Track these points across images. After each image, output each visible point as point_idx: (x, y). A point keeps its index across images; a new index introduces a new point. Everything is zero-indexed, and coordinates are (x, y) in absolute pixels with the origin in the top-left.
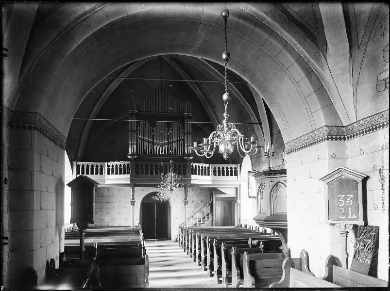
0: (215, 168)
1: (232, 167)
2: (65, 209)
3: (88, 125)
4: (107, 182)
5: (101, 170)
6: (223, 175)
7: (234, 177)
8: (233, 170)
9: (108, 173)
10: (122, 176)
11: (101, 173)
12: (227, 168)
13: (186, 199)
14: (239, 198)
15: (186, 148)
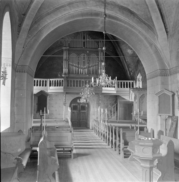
8: (131, 84)
9: (50, 86)
11: (46, 86)
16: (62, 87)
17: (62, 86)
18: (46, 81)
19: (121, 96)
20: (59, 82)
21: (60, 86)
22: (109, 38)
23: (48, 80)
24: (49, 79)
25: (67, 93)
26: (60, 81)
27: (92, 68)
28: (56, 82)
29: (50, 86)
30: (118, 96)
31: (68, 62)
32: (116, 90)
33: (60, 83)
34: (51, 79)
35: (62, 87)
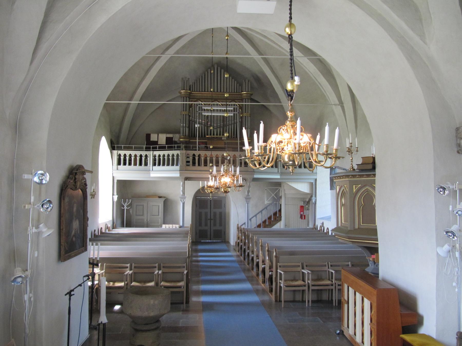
9: (154, 164)
11: (146, 164)
13: (248, 195)
14: (314, 196)
16: (178, 168)
17: (177, 165)
18: (146, 156)
21: (173, 165)
23: (150, 154)
25: (187, 179)
26: (173, 155)
28: (171, 158)
29: (154, 164)
34: (120, 152)
35: (178, 168)
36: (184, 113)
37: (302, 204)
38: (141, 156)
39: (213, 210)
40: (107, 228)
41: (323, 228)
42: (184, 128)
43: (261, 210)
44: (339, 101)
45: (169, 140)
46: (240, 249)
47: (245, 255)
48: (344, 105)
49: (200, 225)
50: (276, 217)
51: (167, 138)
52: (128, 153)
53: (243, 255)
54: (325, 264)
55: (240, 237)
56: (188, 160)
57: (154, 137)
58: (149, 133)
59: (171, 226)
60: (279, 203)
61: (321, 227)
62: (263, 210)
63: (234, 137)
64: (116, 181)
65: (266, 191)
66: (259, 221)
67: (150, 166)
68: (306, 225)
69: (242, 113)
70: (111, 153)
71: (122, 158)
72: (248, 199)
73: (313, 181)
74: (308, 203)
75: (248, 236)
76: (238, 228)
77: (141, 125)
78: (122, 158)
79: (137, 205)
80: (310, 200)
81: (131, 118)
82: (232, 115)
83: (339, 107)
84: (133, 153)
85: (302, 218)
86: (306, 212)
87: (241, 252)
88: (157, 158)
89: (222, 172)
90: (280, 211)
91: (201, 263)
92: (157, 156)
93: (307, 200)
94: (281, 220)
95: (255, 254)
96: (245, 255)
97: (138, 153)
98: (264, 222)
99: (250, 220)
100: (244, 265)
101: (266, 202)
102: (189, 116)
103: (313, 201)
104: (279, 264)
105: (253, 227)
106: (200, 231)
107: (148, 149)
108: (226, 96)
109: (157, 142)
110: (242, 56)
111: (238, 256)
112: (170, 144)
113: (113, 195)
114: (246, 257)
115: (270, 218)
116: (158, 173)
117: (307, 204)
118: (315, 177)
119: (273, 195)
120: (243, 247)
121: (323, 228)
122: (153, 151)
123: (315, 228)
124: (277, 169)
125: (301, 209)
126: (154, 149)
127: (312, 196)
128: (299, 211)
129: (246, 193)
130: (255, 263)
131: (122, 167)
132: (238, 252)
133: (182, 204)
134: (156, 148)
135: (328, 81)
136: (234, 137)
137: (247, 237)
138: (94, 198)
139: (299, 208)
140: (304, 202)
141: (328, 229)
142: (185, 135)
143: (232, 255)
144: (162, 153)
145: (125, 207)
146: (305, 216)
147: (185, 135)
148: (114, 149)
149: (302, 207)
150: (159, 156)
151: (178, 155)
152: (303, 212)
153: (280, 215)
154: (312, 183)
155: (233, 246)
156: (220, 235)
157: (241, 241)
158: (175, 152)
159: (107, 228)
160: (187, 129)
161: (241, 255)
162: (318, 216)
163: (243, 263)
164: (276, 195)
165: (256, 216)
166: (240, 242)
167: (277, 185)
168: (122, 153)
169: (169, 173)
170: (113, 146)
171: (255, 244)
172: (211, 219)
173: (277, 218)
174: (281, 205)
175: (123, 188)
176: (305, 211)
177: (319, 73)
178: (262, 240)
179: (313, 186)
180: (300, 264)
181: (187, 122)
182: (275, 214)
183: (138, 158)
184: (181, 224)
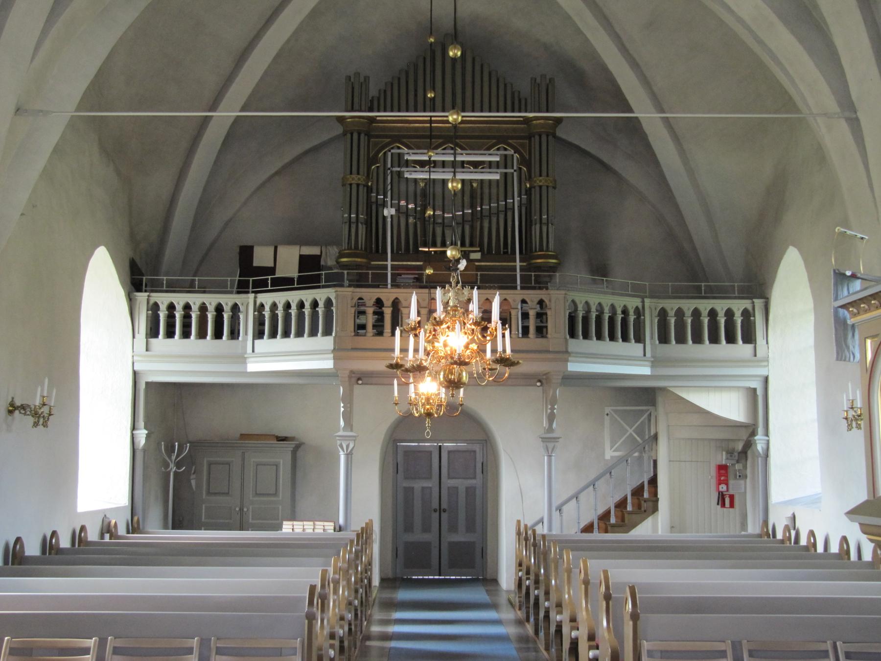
0: (663, 314)
1: (685, 309)
2: (383, 437)
3: (213, 137)
4: (253, 366)
5: (235, 319)
6: (714, 339)
7: (741, 349)
8: (738, 320)
9: (259, 334)
10: (306, 342)
11: (234, 334)
12: (713, 314)
13: (550, 429)
14: (760, 430)
15: (536, 229)
17: (327, 332)
18: (235, 308)
19: (671, 389)
20: (280, 312)
21: (313, 333)
22: (795, 105)
23: (248, 302)
24: (252, 296)
25: (360, 378)
27: (494, 220)
30: (663, 389)
31: (369, 190)
32: (648, 354)
33: (274, 317)
34: (157, 297)
36: (355, 179)
37: (722, 459)
38: (219, 309)
39: (447, 483)
40: (107, 529)
41: (793, 533)
42: (354, 226)
43: (592, 476)
44: (840, 104)
45: (308, 263)
46: (523, 599)
47: (537, 620)
48: (860, 115)
49: (409, 528)
50: (643, 500)
51: (302, 257)
52: (179, 300)
53: (532, 619)
54: (822, 647)
55: (532, 569)
56: (361, 320)
57: (262, 257)
58: (250, 244)
59: (309, 526)
60: (649, 457)
61: (787, 529)
62: (598, 478)
63: (506, 253)
64: (142, 387)
65: (607, 419)
66: (590, 515)
67: (245, 340)
68: (738, 525)
69: (530, 178)
70: (131, 300)
71: (163, 315)
72: (549, 440)
73: (757, 384)
74: (744, 453)
75: (546, 554)
76: (519, 533)
77: (227, 224)
78: (163, 315)
79: (210, 464)
80: (749, 444)
81: (196, 203)
82: (497, 177)
83: (844, 124)
84: (195, 300)
85: (723, 505)
86: (734, 486)
87: (528, 608)
88: (267, 313)
89: (439, 313)
90: (653, 481)
91: (394, 644)
92: (267, 308)
93: (740, 446)
94: (655, 509)
95: (553, 596)
96: (537, 620)
97: (211, 300)
98: (605, 516)
99: (560, 509)
100: (537, 650)
101: (610, 454)
102: (369, 190)
103: (760, 447)
104: (646, 645)
105: (573, 532)
106: (409, 546)
107: (242, 288)
108: (451, 54)
109: (272, 270)
110: (622, 422)
111: (519, 623)
112: (311, 273)
113: (134, 428)
114: (541, 624)
115: (621, 505)
116: (271, 359)
117: (738, 456)
118: (763, 372)
119: (630, 431)
120: (534, 592)
121: (793, 533)
122: (256, 292)
123: (768, 533)
124: (641, 346)
125: (719, 475)
126: (260, 287)
127: (754, 433)
128: (714, 482)
129: (545, 424)
130: (566, 645)
131: (161, 343)
132: (520, 609)
133: (342, 458)
134: (264, 283)
135: (801, 41)
136: (506, 253)
137: (542, 555)
138: (45, 425)
139: (713, 472)
140: (730, 453)
141: (812, 533)
142: (356, 248)
143: (504, 622)
144: (280, 298)
145: (172, 465)
146: (732, 497)
147: (356, 248)
148: (139, 290)
149: (722, 469)
150: (274, 306)
151: (329, 303)
152: (727, 484)
153: (655, 494)
154: (755, 390)
155: (508, 592)
156: (469, 562)
157: (528, 573)
158: (321, 295)
159: (107, 529)
160: (362, 229)
161: (528, 620)
162: (776, 495)
163: (531, 645)
164: (640, 432)
165: (576, 496)
166: (524, 578)
167: (645, 397)
168: (163, 299)
169: (301, 356)
170: (137, 278)
171: (542, 557)
172: (440, 510)
173: (644, 505)
174: (655, 462)
175: (165, 408)
176: (731, 482)
177: (773, 18)
178: (596, 566)
179: (758, 400)
180: (727, 647)
181: (362, 207)
182: (638, 492)
183: (210, 316)
184: (341, 521)
